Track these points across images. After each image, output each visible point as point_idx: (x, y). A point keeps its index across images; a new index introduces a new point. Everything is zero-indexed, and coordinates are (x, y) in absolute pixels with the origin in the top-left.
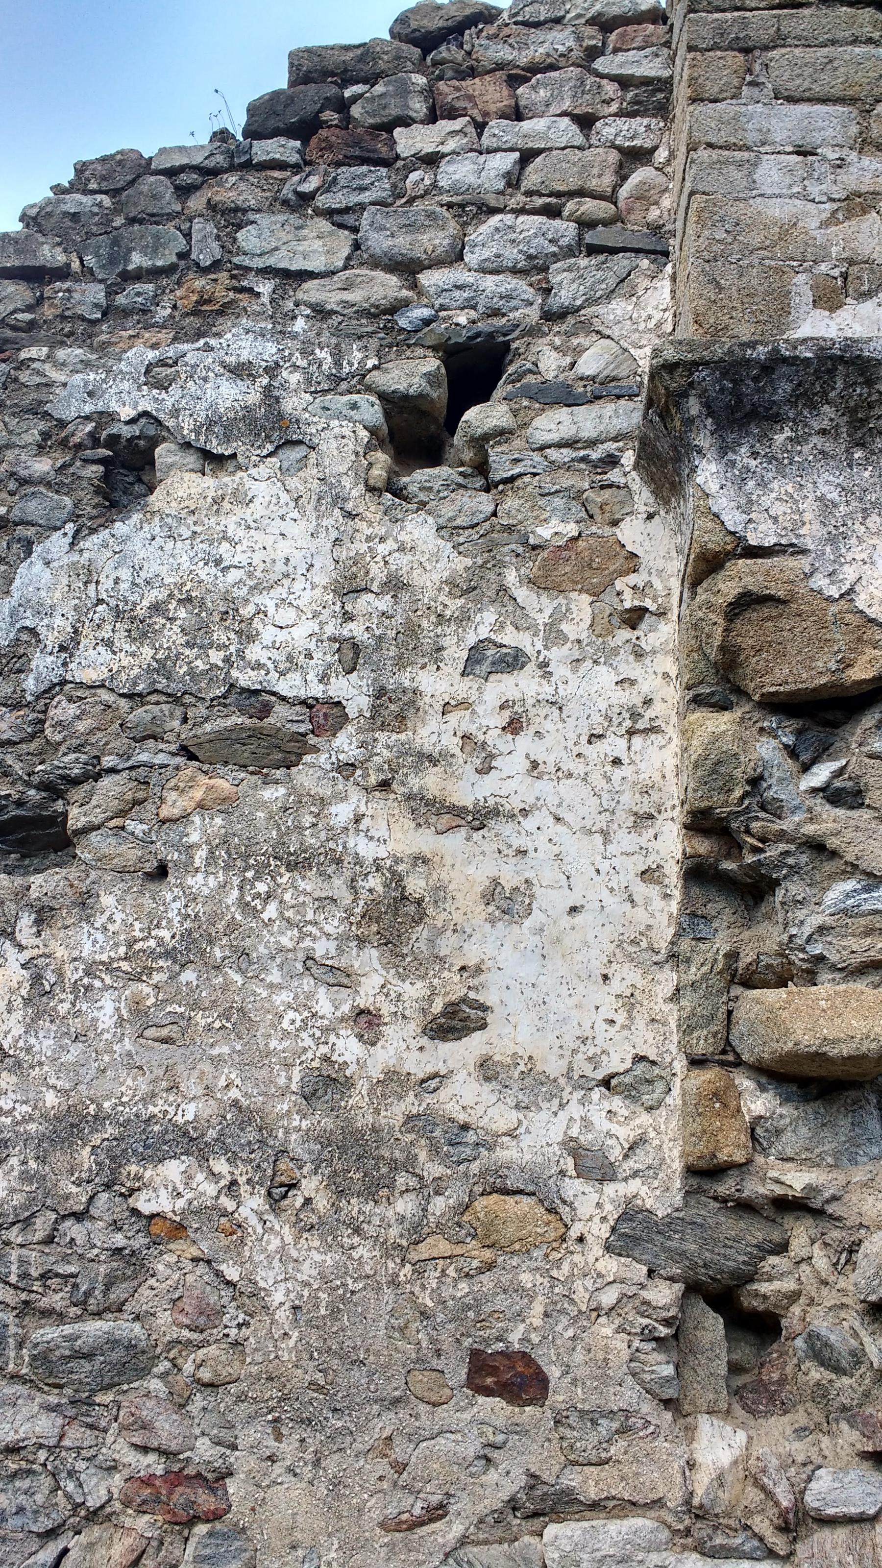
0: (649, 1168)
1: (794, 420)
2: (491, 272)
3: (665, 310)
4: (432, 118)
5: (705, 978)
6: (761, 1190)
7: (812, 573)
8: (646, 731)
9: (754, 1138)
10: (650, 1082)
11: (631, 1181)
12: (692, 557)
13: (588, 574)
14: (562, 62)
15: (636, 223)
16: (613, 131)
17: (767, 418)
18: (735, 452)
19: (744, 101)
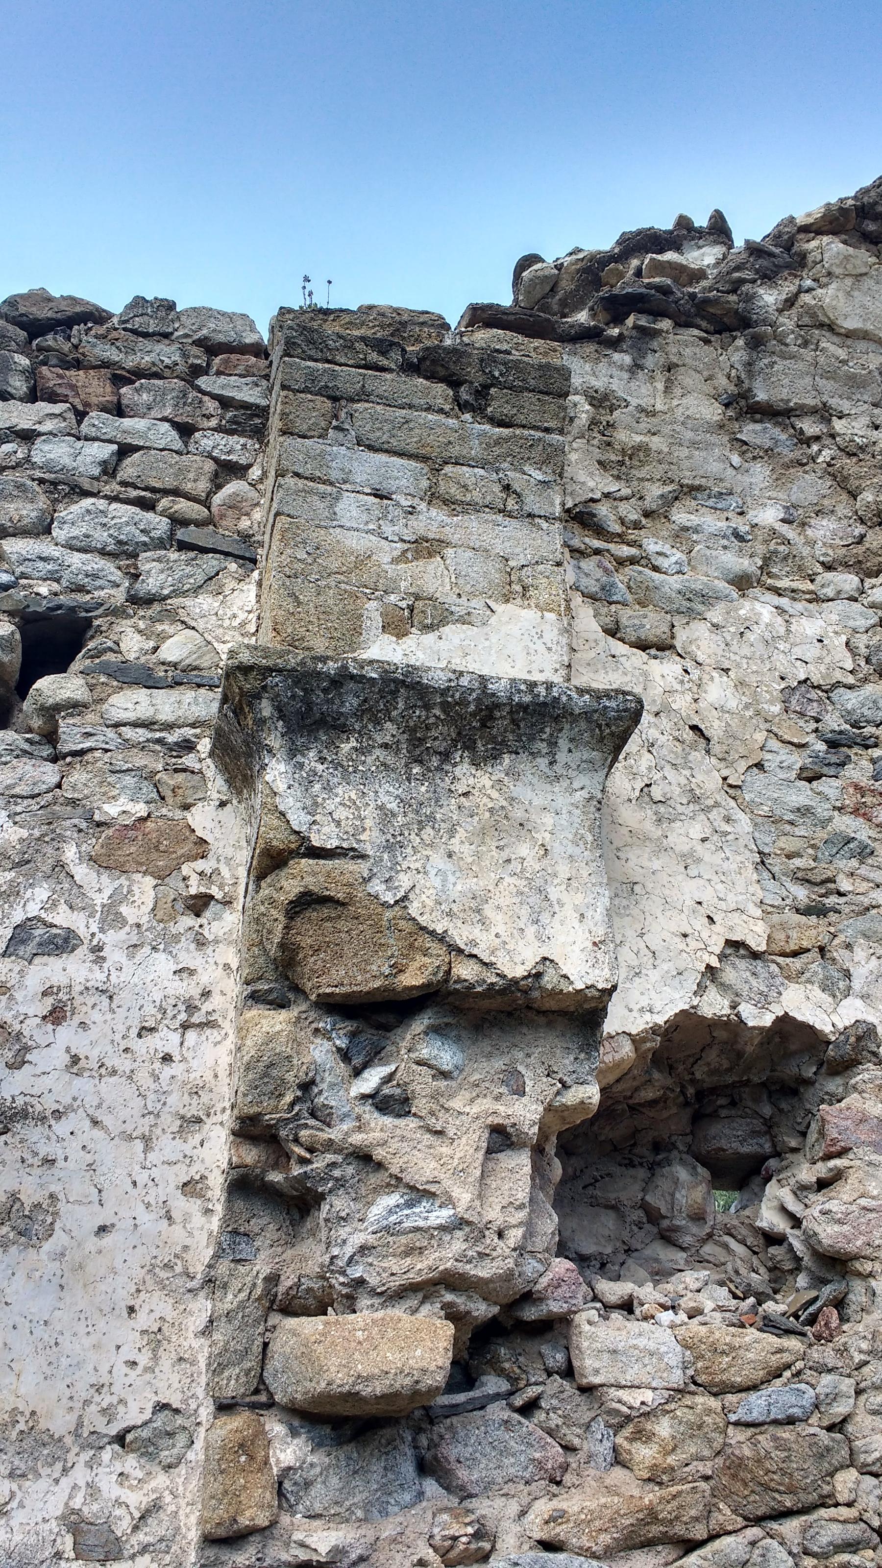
0: (161, 1540)
1: (359, 732)
2: (79, 550)
3: (250, 612)
4: (32, 397)
5: (242, 1306)
6: (285, 1557)
7: (370, 878)
8: (201, 1026)
9: (281, 1493)
10: (170, 1435)
11: (139, 1559)
12: (258, 851)
13: (154, 855)
14: (167, 373)
15: (228, 528)
16: (211, 443)
17: (334, 727)
18: (304, 755)
19: (329, 442)
